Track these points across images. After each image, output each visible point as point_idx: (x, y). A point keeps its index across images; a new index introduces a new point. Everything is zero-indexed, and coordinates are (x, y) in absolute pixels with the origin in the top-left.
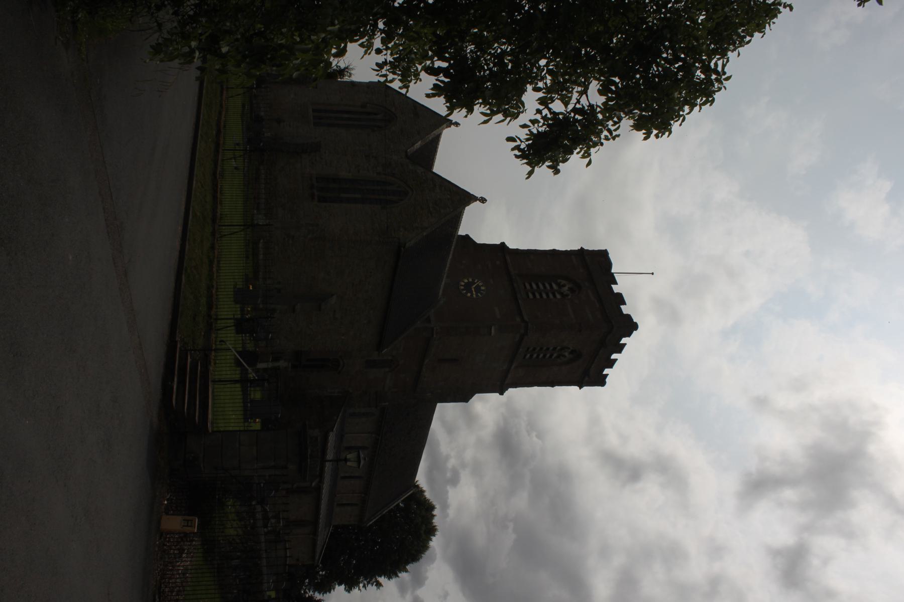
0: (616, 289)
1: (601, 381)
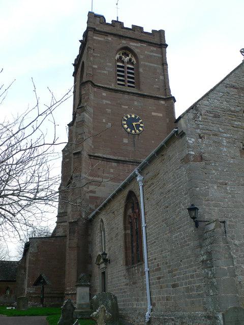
0: (109, 21)
1: (161, 33)
